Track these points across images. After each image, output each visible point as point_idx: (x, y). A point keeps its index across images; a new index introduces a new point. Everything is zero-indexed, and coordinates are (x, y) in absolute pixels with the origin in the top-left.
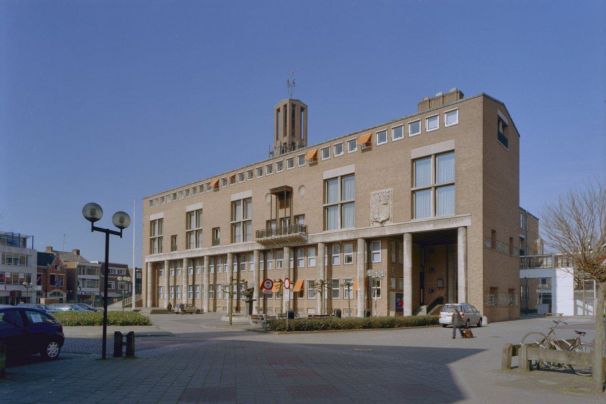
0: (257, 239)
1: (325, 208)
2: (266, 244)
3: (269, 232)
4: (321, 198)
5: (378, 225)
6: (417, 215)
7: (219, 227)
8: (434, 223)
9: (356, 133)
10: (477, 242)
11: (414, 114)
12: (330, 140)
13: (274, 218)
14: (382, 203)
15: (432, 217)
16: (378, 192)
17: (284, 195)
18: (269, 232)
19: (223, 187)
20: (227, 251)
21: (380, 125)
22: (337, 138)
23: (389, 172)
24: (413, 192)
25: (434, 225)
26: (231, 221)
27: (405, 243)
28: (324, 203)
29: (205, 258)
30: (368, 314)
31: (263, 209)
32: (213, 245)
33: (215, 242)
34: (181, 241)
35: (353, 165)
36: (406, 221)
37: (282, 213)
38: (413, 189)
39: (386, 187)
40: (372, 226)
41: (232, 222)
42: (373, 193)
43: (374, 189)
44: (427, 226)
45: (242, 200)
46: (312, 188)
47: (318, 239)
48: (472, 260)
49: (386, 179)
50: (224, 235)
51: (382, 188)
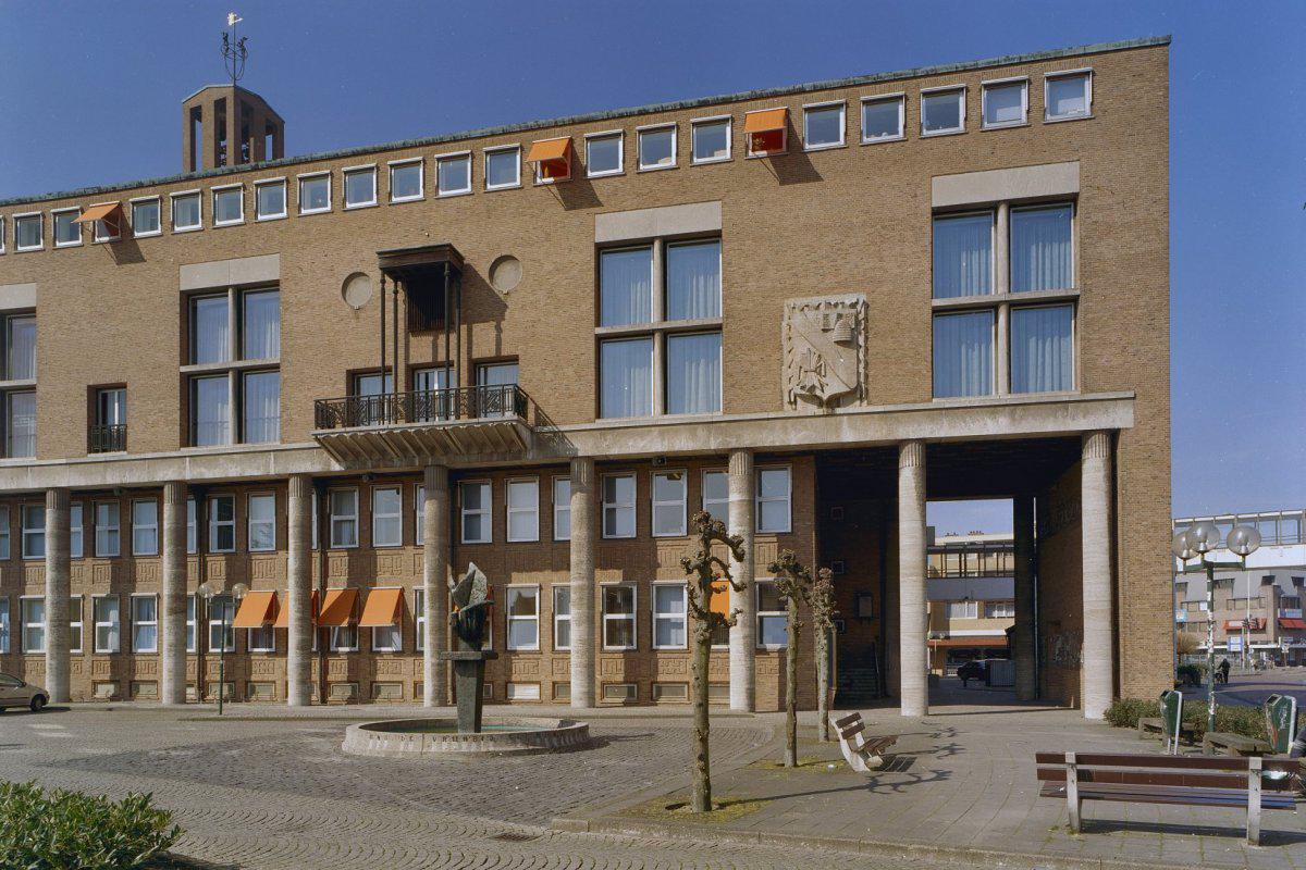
0: (320, 431)
1: (600, 340)
2: (353, 451)
3: (354, 410)
4: (588, 305)
5: (813, 409)
6: (248, 438)
7: (123, 386)
8: (1012, 415)
9: (621, 116)
10: (1155, 478)
11: (941, 68)
12: (622, 110)
13: (442, 357)
14: (836, 335)
15: (1000, 393)
16: (814, 300)
17: (434, 287)
18: (354, 410)
19: (696, 161)
20: (166, 474)
21: (819, 83)
22: (651, 107)
23: (853, 241)
24: (600, 340)
25: (1014, 419)
26: (182, 364)
27: (47, 516)
28: (598, 323)
29: (50, 497)
30: (711, 682)
31: (337, 323)
32: (90, 451)
33: (103, 436)
34: (149, 413)
35: (1074, 168)
36: (915, 402)
37: (422, 349)
38: (599, 331)
39: (844, 287)
40: (788, 411)
41: (184, 369)
42: (791, 302)
43: (796, 290)
44: (989, 421)
45: (657, 245)
46: (548, 267)
47: (585, 447)
48: (1137, 531)
49: (840, 262)
50: (149, 413)
51: (831, 290)
